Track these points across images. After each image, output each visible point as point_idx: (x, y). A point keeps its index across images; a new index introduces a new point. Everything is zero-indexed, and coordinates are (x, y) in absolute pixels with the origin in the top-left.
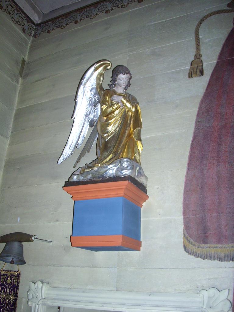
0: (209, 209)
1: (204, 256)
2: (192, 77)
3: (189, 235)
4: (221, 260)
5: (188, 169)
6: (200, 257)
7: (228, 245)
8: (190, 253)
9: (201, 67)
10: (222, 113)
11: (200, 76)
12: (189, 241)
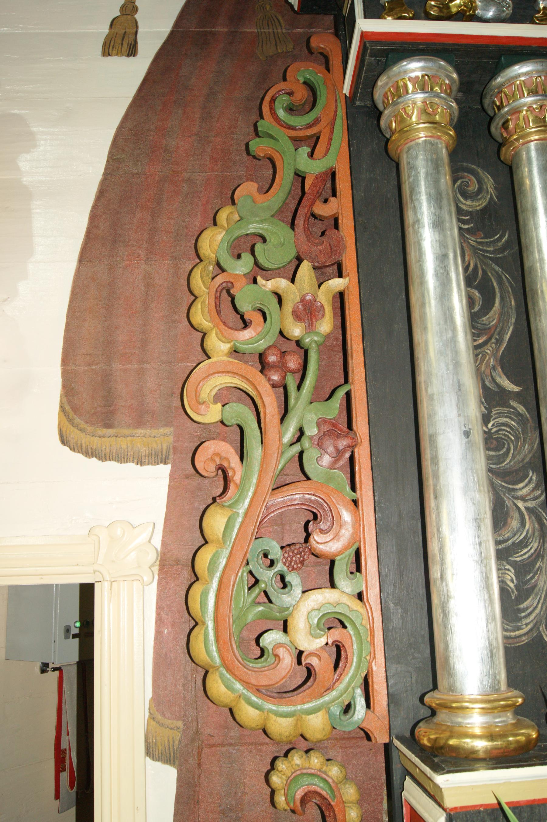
0: (121, 352)
1: (105, 455)
2: (109, 55)
3: (72, 408)
4: (140, 462)
5: (80, 260)
6: (96, 457)
7: (157, 431)
8: (72, 447)
9: (132, 37)
10: (168, 148)
11: (129, 55)
12: (71, 421)
